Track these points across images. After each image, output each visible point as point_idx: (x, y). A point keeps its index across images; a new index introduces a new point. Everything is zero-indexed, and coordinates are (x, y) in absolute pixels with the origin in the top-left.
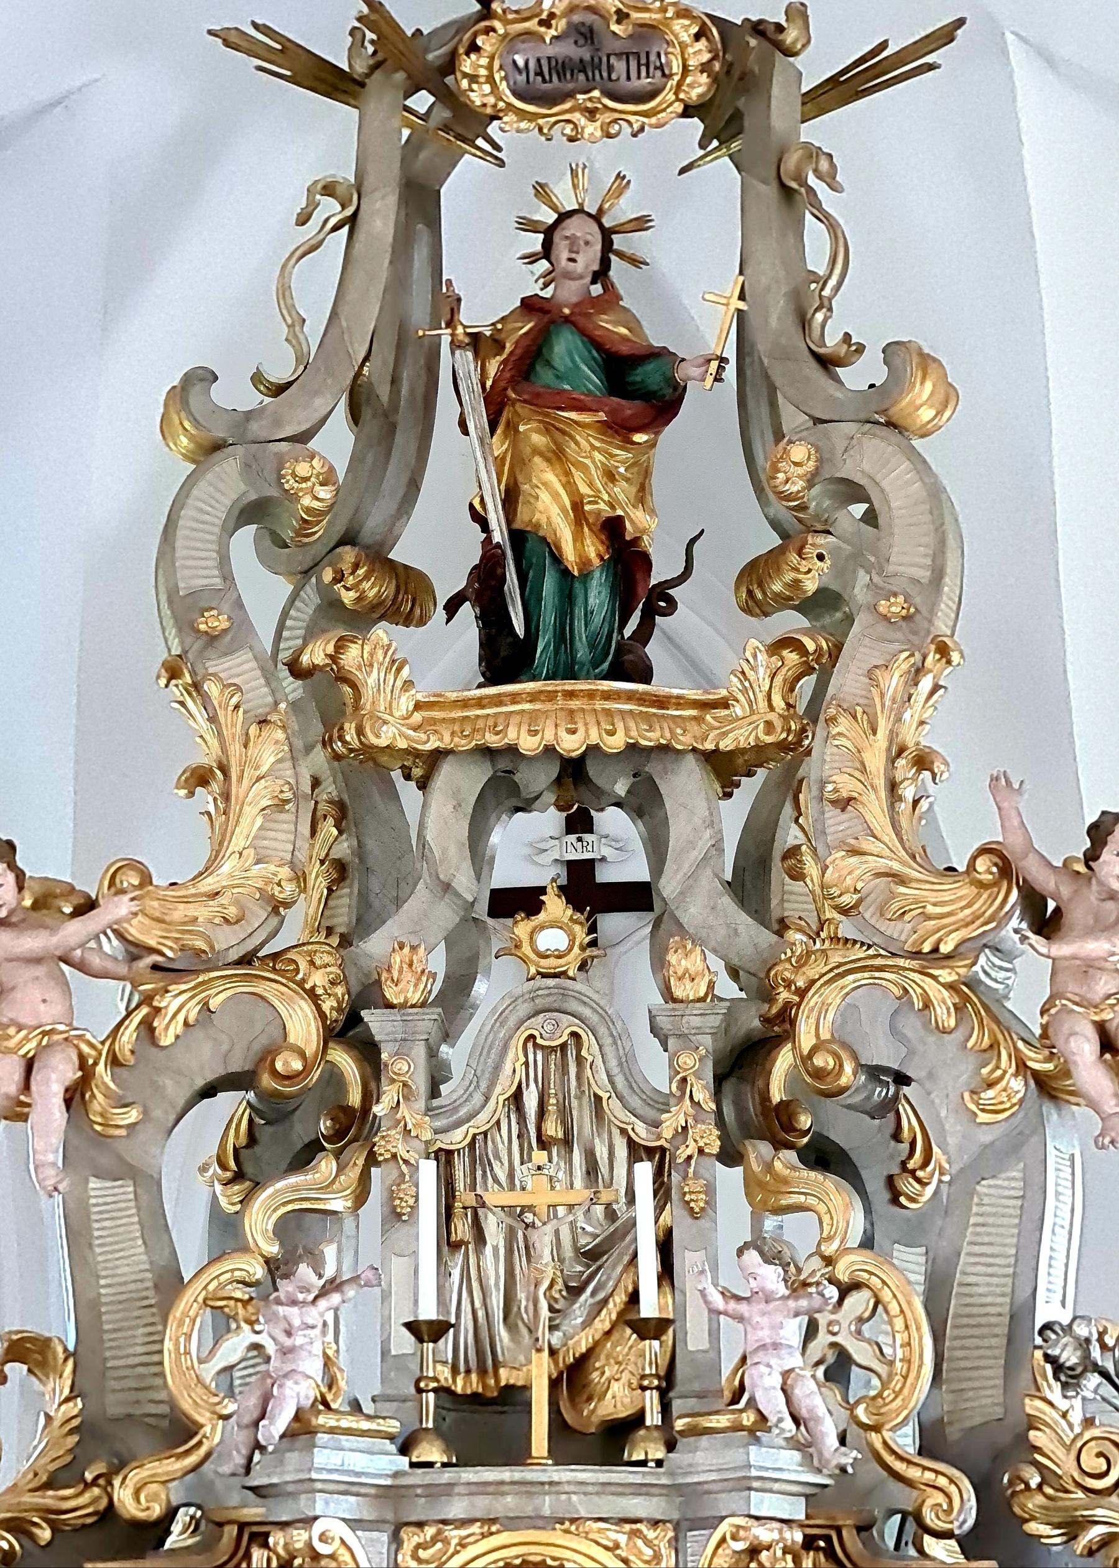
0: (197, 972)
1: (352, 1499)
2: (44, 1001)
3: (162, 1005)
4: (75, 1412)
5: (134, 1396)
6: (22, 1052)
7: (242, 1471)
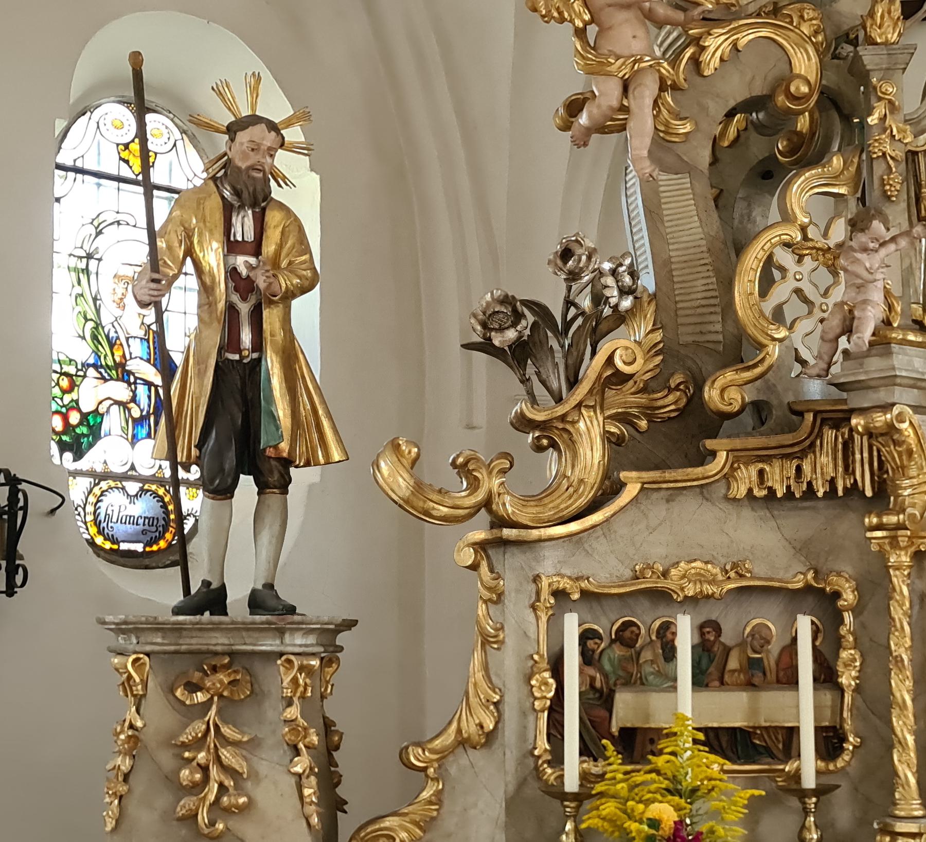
0: (730, 21)
1: (915, 390)
2: (634, 37)
3: (707, 44)
4: (659, 339)
5: (698, 329)
6: (621, 75)
7: (824, 373)
